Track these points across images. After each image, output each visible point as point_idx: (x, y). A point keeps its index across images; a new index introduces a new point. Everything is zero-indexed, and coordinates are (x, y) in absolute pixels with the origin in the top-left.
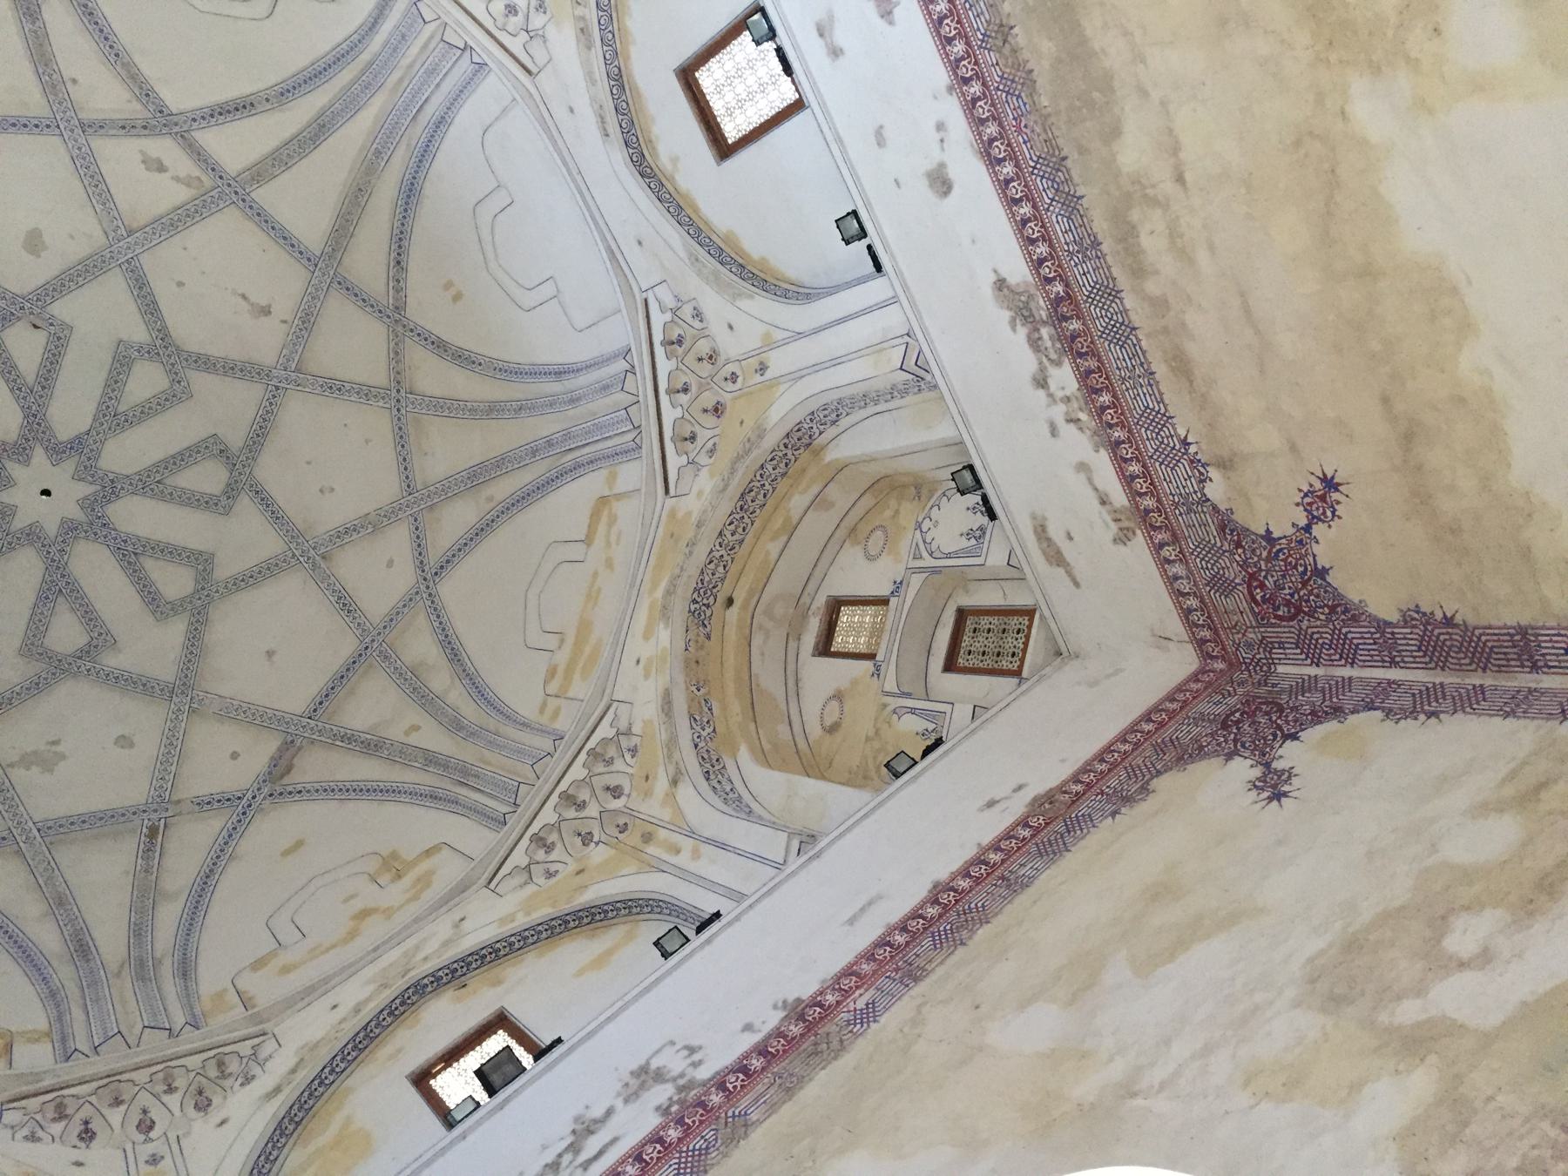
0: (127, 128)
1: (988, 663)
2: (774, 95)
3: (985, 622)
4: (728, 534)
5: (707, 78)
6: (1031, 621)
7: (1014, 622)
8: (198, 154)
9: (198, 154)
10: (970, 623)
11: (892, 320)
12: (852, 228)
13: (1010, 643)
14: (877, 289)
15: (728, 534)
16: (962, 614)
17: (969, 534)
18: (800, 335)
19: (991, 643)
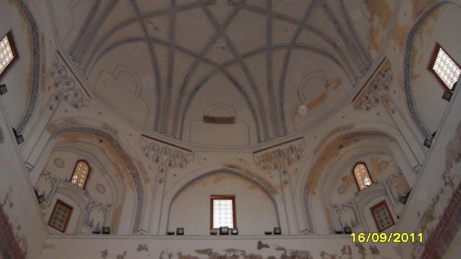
0: (158, 41)
1: (378, 220)
2: (217, 207)
3: (67, 215)
4: (135, 172)
5: (229, 202)
6: (61, 231)
7: (63, 226)
8: (145, 30)
9: (145, 30)
10: (68, 210)
11: (154, 231)
12: (180, 232)
13: (58, 223)
14: (163, 231)
15: (135, 172)
16: (71, 208)
17: (92, 222)
18: (163, 198)
19: (383, 217)
